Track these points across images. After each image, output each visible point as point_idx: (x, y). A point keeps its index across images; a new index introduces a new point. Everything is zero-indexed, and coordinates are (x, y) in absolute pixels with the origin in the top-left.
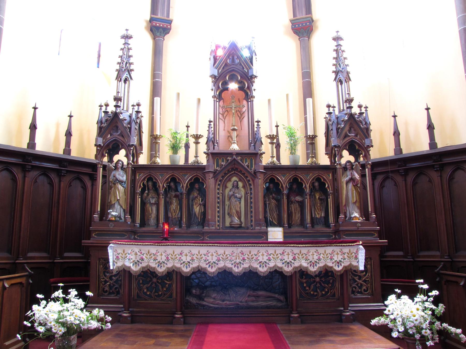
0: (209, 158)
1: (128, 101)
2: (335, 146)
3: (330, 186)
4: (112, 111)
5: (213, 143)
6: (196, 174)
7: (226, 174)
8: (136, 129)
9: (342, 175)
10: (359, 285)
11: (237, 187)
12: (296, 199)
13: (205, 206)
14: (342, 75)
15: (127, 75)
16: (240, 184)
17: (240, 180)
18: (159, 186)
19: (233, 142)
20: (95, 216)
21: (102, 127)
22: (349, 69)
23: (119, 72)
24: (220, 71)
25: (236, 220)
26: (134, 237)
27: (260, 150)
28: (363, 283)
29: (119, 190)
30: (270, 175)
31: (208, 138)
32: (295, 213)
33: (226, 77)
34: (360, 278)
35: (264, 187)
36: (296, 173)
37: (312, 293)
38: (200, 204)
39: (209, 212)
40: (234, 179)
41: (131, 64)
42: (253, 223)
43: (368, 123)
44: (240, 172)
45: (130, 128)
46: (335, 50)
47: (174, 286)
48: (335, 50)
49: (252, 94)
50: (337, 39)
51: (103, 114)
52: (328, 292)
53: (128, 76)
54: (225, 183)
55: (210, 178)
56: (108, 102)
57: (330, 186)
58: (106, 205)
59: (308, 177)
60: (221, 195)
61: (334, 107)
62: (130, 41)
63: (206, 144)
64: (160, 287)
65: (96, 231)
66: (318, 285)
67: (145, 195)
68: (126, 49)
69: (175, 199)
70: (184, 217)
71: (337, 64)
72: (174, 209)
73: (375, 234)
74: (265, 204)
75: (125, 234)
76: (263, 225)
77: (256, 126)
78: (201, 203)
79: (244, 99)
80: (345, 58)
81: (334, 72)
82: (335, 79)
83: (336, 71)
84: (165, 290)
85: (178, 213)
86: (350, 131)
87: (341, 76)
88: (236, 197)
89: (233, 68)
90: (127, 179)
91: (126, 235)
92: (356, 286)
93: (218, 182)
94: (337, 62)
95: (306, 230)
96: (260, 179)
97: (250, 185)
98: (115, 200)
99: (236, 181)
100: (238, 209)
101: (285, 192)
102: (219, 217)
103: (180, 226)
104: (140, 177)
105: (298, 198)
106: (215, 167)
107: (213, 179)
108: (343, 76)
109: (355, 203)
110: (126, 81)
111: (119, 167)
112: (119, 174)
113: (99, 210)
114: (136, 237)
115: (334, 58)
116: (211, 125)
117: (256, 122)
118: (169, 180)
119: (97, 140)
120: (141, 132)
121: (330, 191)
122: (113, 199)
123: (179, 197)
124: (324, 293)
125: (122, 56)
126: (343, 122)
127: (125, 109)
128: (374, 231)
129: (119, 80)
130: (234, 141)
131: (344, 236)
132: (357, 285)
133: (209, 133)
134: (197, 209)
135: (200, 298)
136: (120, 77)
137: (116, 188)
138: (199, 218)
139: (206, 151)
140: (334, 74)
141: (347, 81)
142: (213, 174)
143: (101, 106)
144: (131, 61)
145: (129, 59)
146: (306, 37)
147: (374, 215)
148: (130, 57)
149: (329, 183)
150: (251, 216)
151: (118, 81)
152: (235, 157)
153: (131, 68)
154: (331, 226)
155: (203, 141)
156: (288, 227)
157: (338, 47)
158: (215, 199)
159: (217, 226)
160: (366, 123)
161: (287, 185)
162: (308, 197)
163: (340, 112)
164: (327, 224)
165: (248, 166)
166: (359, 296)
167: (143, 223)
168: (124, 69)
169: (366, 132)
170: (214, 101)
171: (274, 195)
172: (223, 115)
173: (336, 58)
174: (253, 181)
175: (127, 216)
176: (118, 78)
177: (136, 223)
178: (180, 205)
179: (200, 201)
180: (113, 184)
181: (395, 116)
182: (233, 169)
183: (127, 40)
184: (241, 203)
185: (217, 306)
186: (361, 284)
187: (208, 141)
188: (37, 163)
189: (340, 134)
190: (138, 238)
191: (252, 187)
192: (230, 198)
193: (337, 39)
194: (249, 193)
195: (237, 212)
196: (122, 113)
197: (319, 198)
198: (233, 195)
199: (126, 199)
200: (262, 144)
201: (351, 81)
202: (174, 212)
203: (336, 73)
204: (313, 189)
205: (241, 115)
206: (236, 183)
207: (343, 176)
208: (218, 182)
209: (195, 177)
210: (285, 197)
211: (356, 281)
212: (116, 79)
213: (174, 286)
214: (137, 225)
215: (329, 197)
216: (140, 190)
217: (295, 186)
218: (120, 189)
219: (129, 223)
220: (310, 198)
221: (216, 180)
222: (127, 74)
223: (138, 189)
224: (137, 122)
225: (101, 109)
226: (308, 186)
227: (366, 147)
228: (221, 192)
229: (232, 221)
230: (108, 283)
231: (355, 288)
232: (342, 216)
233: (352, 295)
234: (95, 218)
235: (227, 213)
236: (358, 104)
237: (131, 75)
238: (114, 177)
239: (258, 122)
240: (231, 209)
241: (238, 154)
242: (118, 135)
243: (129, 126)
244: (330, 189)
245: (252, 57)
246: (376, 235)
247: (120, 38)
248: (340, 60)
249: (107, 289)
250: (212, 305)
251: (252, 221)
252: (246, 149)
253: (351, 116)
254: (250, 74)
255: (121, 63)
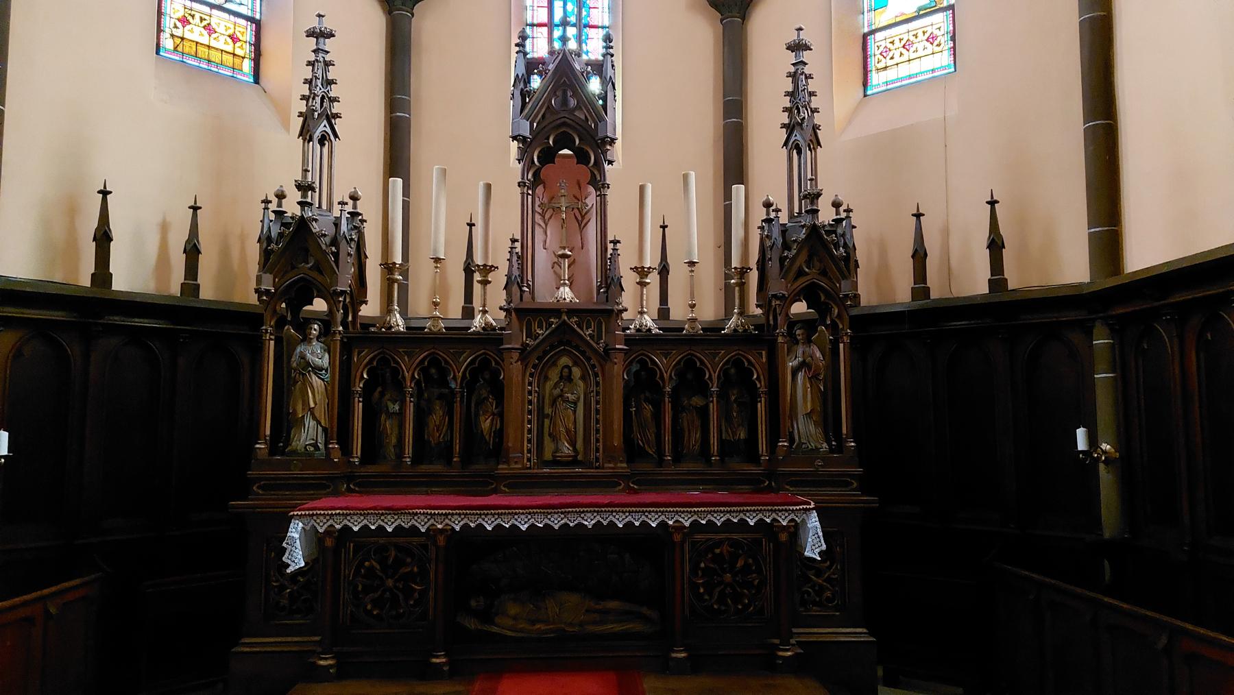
0: (510, 319)
1: (331, 189)
2: (775, 296)
3: (762, 377)
4: (294, 214)
5: (520, 288)
6: (483, 351)
7: (545, 353)
8: (349, 255)
9: (788, 355)
10: (817, 588)
11: (569, 379)
12: (691, 402)
13: (501, 415)
14: (801, 135)
15: (324, 129)
16: (577, 372)
17: (576, 364)
18: (404, 377)
19: (562, 282)
20: (258, 446)
21: (272, 250)
22: (818, 119)
23: (308, 119)
24: (535, 124)
25: (566, 449)
26: (348, 486)
27: (618, 304)
28: (825, 584)
29: (312, 386)
30: (639, 353)
31: (509, 276)
32: (689, 430)
33: (548, 138)
34: (819, 573)
35: (626, 377)
36: (690, 350)
37: (702, 565)
38: (493, 414)
39: (511, 433)
40: (565, 360)
41: (334, 100)
42: (600, 454)
43: (851, 246)
44: (577, 348)
45: (336, 255)
46: (789, 75)
47: (431, 594)
48: (789, 75)
49: (605, 180)
50: (798, 47)
51: (272, 217)
52: (749, 605)
53: (329, 130)
54: (545, 370)
55: (513, 361)
56: (284, 189)
57: (762, 377)
58: (285, 423)
59: (717, 359)
60: (536, 395)
61: (777, 210)
62: (328, 44)
63: (505, 288)
64: (401, 597)
65: (260, 479)
66: (728, 590)
67: (376, 394)
68: (320, 63)
69: (437, 401)
70: (458, 441)
71: (793, 107)
72: (437, 423)
73: (853, 481)
74: (627, 416)
75: (327, 484)
76: (621, 459)
77: (610, 251)
78: (496, 411)
79: (588, 184)
80: (812, 94)
81: (784, 126)
82: (786, 144)
83: (789, 124)
84: (411, 605)
85: (447, 430)
86: (809, 262)
87: (799, 137)
88: (567, 401)
89: (563, 120)
90: (331, 362)
91: (329, 487)
92: (810, 590)
93: (530, 370)
94: (793, 102)
95: (710, 469)
96: (616, 364)
97: (596, 375)
98: (303, 409)
99: (567, 366)
100: (571, 426)
101: (668, 389)
102: (529, 441)
103: (449, 462)
104: (362, 359)
105: (697, 401)
106: (524, 339)
107: (519, 363)
108: (803, 139)
109: (809, 415)
110: (322, 140)
111: (311, 337)
112: (312, 353)
113: (268, 432)
114: (351, 486)
115: (788, 94)
116: (515, 248)
117: (611, 242)
118: (426, 363)
119: (259, 280)
120: (363, 257)
121: (762, 386)
122: (299, 408)
123: (448, 400)
124: (740, 607)
125: (311, 80)
126: (796, 244)
127: (324, 207)
128: (852, 476)
129: (306, 138)
130: (564, 280)
131: (787, 485)
132: (813, 587)
133: (511, 266)
134: (486, 424)
135: (486, 616)
136: (308, 131)
137: (307, 383)
138: (489, 444)
139: (503, 303)
140: (784, 130)
141: (812, 146)
142: (518, 354)
143: (267, 202)
144: (332, 94)
145: (329, 88)
146: (736, 17)
147: (851, 442)
148: (330, 82)
149: (759, 370)
150: (598, 441)
151: (304, 140)
152: (566, 318)
153: (334, 111)
154: (761, 461)
155: (499, 279)
156: (671, 462)
157: (797, 67)
158: (523, 405)
159: (525, 461)
160: (845, 246)
161: (673, 374)
162: (715, 399)
163: (791, 218)
164: (754, 458)
165: (591, 336)
166: (815, 611)
167: (367, 457)
168: (319, 114)
169: (848, 264)
170: (522, 194)
171: (647, 394)
172: (543, 216)
173: (791, 94)
174: (601, 365)
175: (331, 446)
176: (305, 133)
177: (353, 457)
178: (450, 413)
179: (492, 406)
180: (300, 374)
181: (918, 216)
182: (561, 343)
183: (321, 40)
184: (577, 411)
185: (519, 635)
186: (821, 586)
187: (509, 283)
188: (117, 320)
189: (786, 271)
190: (357, 489)
191: (600, 379)
192: (553, 403)
193: (798, 47)
194: (593, 391)
195: (568, 431)
196: (316, 220)
197: (735, 400)
198: (561, 396)
199: (330, 406)
200: (623, 290)
201: (821, 147)
202: (438, 431)
203: (790, 128)
204: (726, 381)
205: (583, 217)
206: (566, 370)
207: (789, 357)
208: (530, 370)
209: (482, 357)
210: (667, 399)
211: (811, 580)
212: (301, 134)
213: (431, 594)
214: (354, 462)
215: (759, 399)
216: (361, 385)
217: (689, 376)
218: (315, 385)
219: (335, 460)
220: (717, 402)
221: (526, 366)
222: (325, 126)
223: (357, 384)
224: (352, 239)
225: (266, 208)
226: (715, 376)
227: (842, 298)
228: (537, 389)
229: (557, 450)
230: (288, 591)
231: (809, 594)
232: (783, 443)
233: (802, 609)
234: (258, 450)
235: (547, 433)
236: (833, 198)
237: (336, 127)
238: (301, 358)
239: (615, 242)
240: (555, 425)
241: (572, 311)
242: (310, 269)
243: (333, 249)
244: (763, 383)
245: (606, 92)
246: (855, 485)
247: (305, 34)
248: (800, 100)
249: (284, 602)
250: (509, 633)
251: (597, 450)
252: (594, 301)
253: (814, 230)
254: (600, 135)
255: (309, 97)
